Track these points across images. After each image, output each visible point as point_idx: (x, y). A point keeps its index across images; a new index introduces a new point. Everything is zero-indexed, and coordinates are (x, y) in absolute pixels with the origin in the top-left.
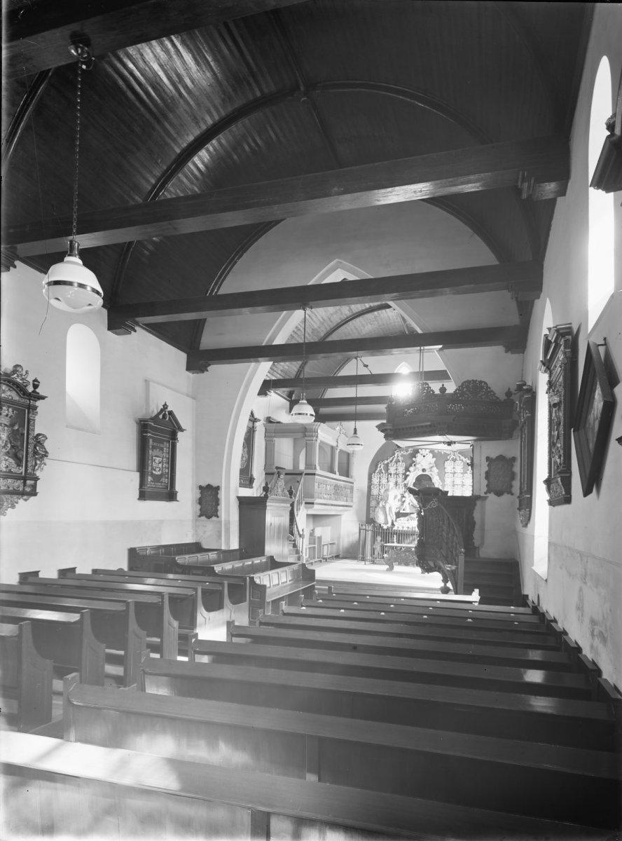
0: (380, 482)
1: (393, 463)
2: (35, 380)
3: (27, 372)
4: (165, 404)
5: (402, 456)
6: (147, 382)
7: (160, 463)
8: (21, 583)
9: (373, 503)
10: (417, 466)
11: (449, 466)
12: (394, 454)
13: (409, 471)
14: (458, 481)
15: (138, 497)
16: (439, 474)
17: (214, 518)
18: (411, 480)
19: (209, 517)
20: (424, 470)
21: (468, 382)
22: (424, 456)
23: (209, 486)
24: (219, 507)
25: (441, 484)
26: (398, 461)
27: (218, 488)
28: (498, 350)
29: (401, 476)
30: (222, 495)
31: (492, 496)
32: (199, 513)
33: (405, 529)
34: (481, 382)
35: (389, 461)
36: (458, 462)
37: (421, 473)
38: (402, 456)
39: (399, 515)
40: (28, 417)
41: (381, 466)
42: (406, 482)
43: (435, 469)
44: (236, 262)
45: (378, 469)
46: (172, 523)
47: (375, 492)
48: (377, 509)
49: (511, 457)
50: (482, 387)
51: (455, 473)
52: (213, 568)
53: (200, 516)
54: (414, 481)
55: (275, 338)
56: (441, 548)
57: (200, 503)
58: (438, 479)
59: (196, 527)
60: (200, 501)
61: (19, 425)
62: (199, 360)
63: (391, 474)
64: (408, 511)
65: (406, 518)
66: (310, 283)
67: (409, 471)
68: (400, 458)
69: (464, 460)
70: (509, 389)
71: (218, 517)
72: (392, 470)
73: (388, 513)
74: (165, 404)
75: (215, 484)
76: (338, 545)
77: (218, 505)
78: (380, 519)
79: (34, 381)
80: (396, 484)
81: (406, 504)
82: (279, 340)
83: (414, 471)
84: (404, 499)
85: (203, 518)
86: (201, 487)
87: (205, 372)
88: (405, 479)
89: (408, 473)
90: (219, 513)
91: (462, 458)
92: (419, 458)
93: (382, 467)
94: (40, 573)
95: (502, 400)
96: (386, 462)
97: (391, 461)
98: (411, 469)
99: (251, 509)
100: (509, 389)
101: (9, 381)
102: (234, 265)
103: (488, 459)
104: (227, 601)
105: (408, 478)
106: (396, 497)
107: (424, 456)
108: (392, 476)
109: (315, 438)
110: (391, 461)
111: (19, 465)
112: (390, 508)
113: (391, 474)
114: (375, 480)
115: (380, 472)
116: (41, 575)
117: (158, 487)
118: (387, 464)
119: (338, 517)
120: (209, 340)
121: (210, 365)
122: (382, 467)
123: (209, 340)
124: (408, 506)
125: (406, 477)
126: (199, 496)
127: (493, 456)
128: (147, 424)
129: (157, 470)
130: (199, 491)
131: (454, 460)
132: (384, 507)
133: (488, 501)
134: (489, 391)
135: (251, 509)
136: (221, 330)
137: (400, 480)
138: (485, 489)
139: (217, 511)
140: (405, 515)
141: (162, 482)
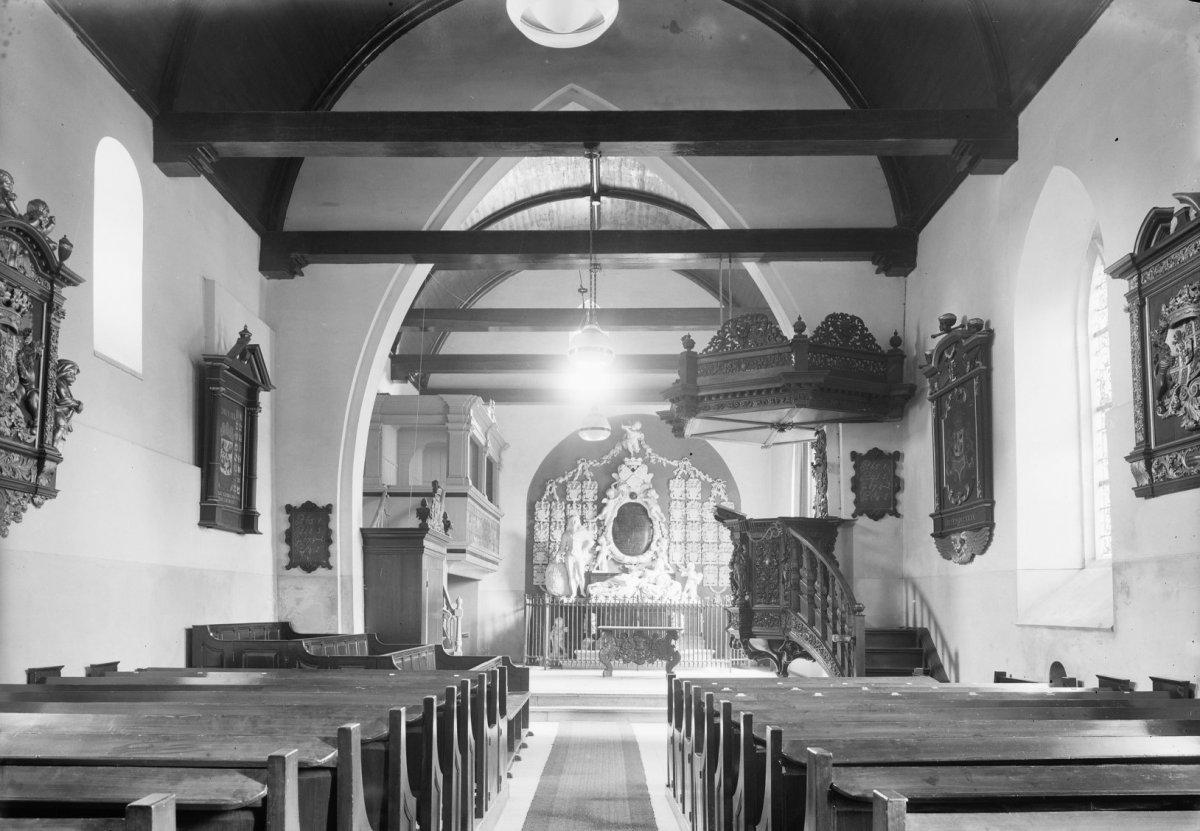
0: (551, 517)
1: (575, 482)
2: (64, 241)
3: (51, 221)
4: (245, 330)
5: (591, 468)
6: (208, 285)
7: (229, 452)
8: (89, 675)
9: (539, 557)
10: (622, 488)
11: (676, 488)
12: (576, 466)
13: (606, 496)
14: (694, 515)
15: (197, 519)
16: (660, 502)
17: (321, 571)
18: (610, 512)
19: (309, 568)
20: (633, 495)
21: (834, 316)
22: (633, 470)
23: (309, 507)
24: (331, 548)
25: (665, 519)
26: (583, 479)
27: (329, 509)
28: (866, 267)
29: (590, 505)
30: (337, 523)
31: (864, 521)
32: (286, 561)
33: (611, 601)
34: (853, 318)
35: (566, 478)
36: (693, 481)
37: (628, 500)
38: (591, 468)
39: (590, 578)
40: (48, 318)
41: (552, 488)
42: (600, 517)
43: (653, 493)
44: (363, 68)
45: (547, 493)
46: (246, 581)
47: (541, 535)
48: (550, 568)
49: (892, 452)
50: (856, 327)
51: (687, 501)
52: (390, 658)
53: (288, 568)
54: (615, 515)
55: (445, 220)
56: (799, 610)
57: (288, 541)
58: (659, 511)
59: (279, 591)
60: (289, 538)
61: (34, 336)
62: (286, 251)
63: (571, 503)
64: (605, 570)
65: (606, 583)
66: (535, 109)
67: (606, 496)
68: (588, 474)
69: (703, 477)
70: (896, 333)
71: (330, 568)
72: (573, 495)
73: (571, 574)
74: (245, 330)
75: (321, 503)
76: (474, 637)
77: (329, 541)
78: (557, 585)
79: (61, 242)
80: (582, 518)
81: (602, 558)
82: (460, 220)
83: (616, 497)
84: (598, 548)
85: (297, 571)
86: (289, 509)
87: (297, 277)
88: (599, 511)
89: (604, 501)
90: (331, 561)
91: (699, 473)
92: (624, 473)
93: (554, 489)
94: (119, 666)
95: (886, 352)
96: (561, 481)
97: (571, 479)
98: (611, 493)
99: (394, 551)
100: (896, 333)
101: (26, 235)
102: (358, 72)
103: (854, 455)
104: (919, 634)
105: (605, 511)
106: (585, 544)
107: (633, 470)
108: (574, 505)
109: (465, 426)
110: (571, 479)
111: (30, 426)
112: (576, 565)
113: (571, 503)
114: (542, 514)
115: (551, 499)
116: (64, 673)
117: (226, 505)
118: (565, 484)
119: (474, 583)
120: (302, 213)
121: (307, 263)
122: (554, 489)
123: (302, 213)
124: (605, 561)
125: (600, 508)
126: (286, 526)
127: (863, 450)
128: (219, 367)
129: (226, 465)
130: (285, 516)
131: (686, 477)
132: (564, 565)
133: (856, 530)
134: (867, 338)
135: (394, 551)
136: (348, 188)
137: (589, 513)
138: (852, 509)
139: (328, 555)
140: (603, 577)
141: (232, 493)
